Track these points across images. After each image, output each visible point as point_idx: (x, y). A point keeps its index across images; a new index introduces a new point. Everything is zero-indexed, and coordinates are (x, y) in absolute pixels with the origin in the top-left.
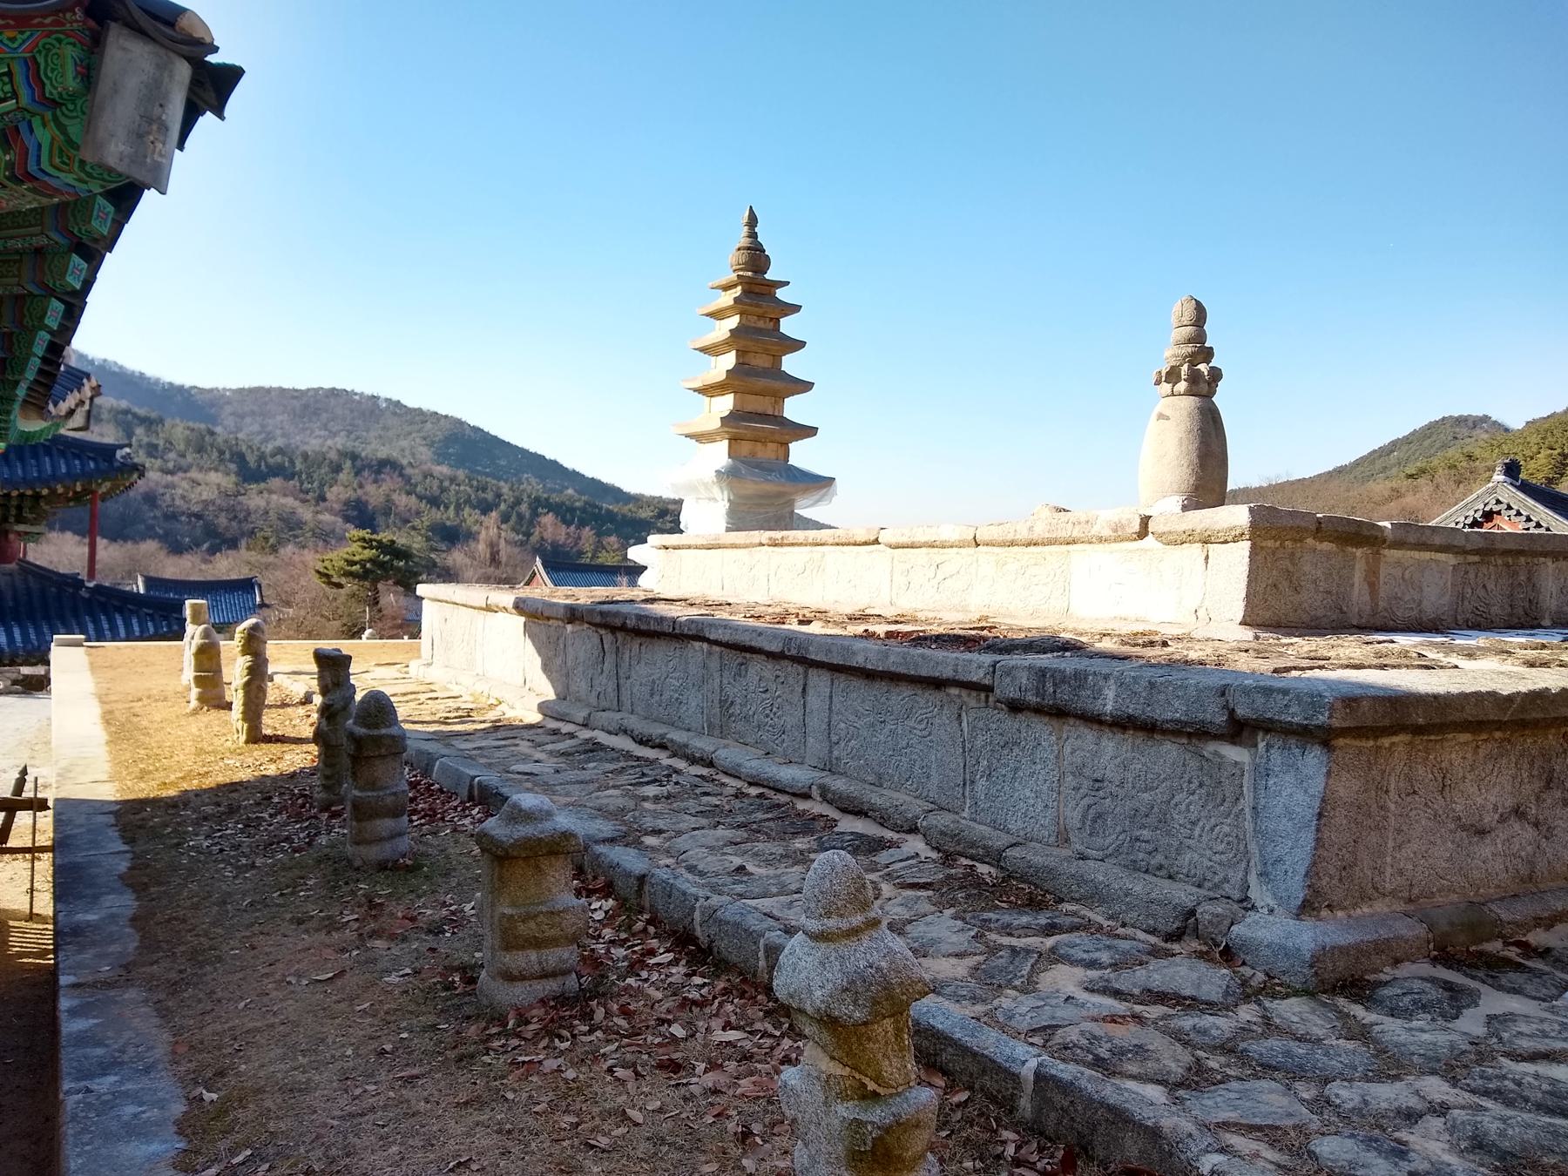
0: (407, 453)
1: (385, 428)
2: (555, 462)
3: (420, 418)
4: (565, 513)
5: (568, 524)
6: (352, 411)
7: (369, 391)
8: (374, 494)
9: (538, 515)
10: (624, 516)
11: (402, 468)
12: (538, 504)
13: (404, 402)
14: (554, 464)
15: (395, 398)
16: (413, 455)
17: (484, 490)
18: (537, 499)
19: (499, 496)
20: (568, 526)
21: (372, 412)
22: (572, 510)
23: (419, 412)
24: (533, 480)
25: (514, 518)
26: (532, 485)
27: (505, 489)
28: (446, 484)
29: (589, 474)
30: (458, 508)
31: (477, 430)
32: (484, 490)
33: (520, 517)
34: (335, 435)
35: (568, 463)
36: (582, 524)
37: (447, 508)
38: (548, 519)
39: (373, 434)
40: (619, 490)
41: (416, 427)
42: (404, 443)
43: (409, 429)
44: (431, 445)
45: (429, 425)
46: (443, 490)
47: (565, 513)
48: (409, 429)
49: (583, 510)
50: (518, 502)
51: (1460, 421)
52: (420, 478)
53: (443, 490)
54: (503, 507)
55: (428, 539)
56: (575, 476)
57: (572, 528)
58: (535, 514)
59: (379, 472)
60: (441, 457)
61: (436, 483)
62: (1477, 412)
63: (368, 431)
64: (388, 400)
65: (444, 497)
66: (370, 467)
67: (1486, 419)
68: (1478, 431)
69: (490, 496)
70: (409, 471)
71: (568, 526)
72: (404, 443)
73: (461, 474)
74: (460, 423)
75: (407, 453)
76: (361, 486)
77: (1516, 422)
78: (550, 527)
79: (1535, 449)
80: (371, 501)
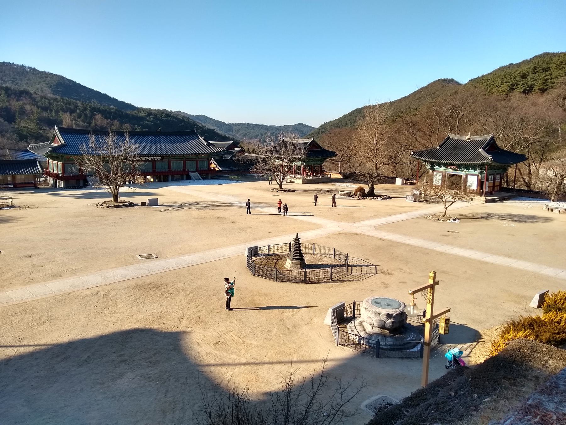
0: (40, 90)
1: (29, 80)
2: (105, 95)
3: (44, 75)
4: (106, 114)
5: (107, 119)
6: (13, 72)
7: (21, 63)
8: (15, 105)
9: (94, 115)
10: (133, 115)
11: (31, 94)
12: (94, 110)
13: (37, 68)
14: (105, 95)
15: (33, 67)
16: (42, 91)
17: (70, 104)
18: (94, 108)
19: (76, 107)
20: (107, 119)
21: (23, 73)
22: (110, 113)
23: (44, 73)
24: (96, 102)
25: (83, 116)
26: (95, 103)
27: (79, 104)
28: (52, 101)
29: (120, 100)
30: (57, 112)
31: (71, 81)
32: (70, 104)
33: (86, 115)
34: (6, 82)
35: (111, 95)
36: (114, 119)
37: (51, 112)
38: (98, 116)
39: (23, 82)
40: (133, 106)
41: (43, 80)
42: (38, 86)
43: (40, 80)
44: (50, 87)
45: (49, 79)
46: (50, 104)
47: (106, 114)
48: (40, 80)
49: (115, 113)
50: (85, 109)
51: (445, 81)
52: (39, 99)
53: (50, 104)
54: (78, 111)
55: (37, 124)
56: (114, 101)
57: (109, 120)
58: (93, 114)
59: (20, 96)
60: (55, 92)
61: (47, 101)
62: (450, 78)
63: (21, 81)
64: (30, 68)
65: (51, 107)
66: (15, 94)
67: (452, 80)
68: (450, 84)
69: (72, 107)
70: (34, 96)
71: (107, 119)
72: (38, 86)
73: (59, 98)
74: (62, 78)
75: (40, 90)
76: (8, 101)
77: (463, 79)
78: (99, 119)
79: (500, 83)
80: (13, 108)
